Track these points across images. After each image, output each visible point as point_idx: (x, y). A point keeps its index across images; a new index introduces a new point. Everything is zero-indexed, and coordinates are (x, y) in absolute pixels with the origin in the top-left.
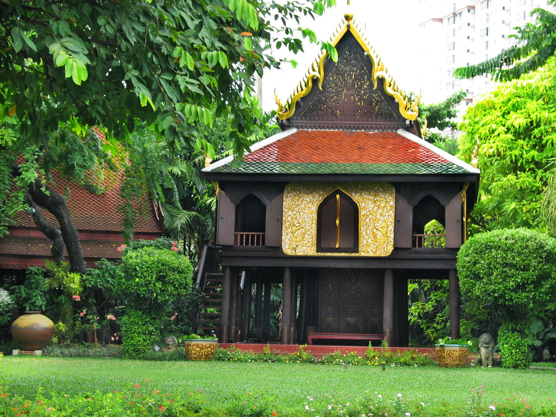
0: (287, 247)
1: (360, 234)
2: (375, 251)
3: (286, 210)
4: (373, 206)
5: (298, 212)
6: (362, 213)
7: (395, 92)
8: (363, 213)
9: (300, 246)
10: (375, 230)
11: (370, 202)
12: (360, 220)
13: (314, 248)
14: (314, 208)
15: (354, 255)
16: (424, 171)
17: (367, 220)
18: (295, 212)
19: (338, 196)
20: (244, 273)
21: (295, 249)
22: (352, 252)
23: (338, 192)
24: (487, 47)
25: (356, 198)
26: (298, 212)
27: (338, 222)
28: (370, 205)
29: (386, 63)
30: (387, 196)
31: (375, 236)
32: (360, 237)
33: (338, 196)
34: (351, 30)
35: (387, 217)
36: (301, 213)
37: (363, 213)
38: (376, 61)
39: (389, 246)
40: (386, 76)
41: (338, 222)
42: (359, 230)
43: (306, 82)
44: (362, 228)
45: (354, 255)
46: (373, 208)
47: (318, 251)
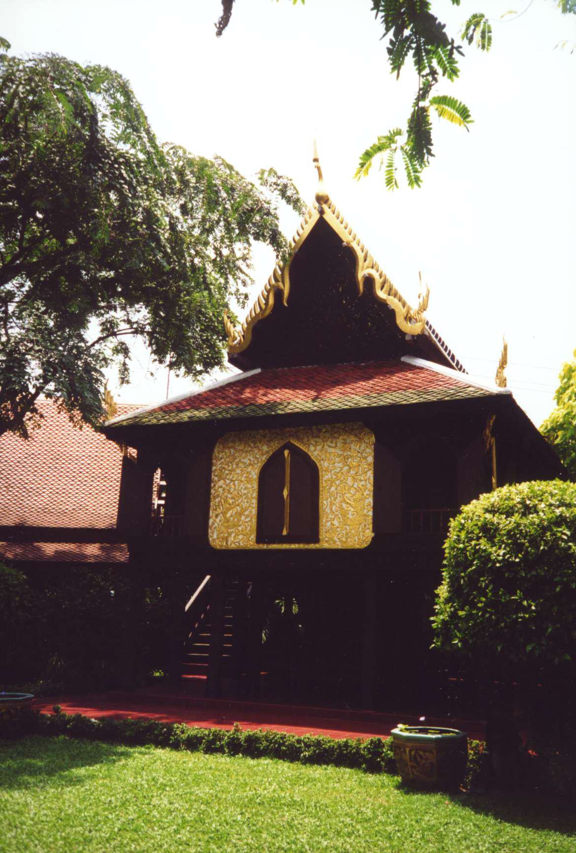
0: (215, 537)
1: (321, 513)
2: (344, 539)
3: (216, 479)
4: (341, 465)
5: (232, 480)
6: (325, 478)
7: (391, 297)
8: (326, 477)
9: (233, 535)
10: (344, 505)
11: (337, 459)
12: (321, 489)
13: (253, 537)
14: (255, 474)
15: (312, 546)
16: (415, 400)
17: (333, 489)
18: (228, 482)
19: (286, 452)
20: (205, 677)
21: (227, 539)
22: (309, 542)
23: (289, 446)
24: (315, 143)
25: (316, 453)
26: (232, 480)
27: (285, 493)
28: (336, 465)
29: (376, 255)
30: (362, 448)
31: (344, 514)
32: (321, 516)
33: (286, 452)
34: (325, 216)
35: (363, 483)
36: (236, 482)
37: (326, 477)
38: (360, 255)
39: (367, 531)
40: (376, 275)
41: (285, 493)
42: (320, 505)
43: (263, 307)
44: (325, 502)
45: (312, 546)
46: (341, 469)
47: (259, 540)
